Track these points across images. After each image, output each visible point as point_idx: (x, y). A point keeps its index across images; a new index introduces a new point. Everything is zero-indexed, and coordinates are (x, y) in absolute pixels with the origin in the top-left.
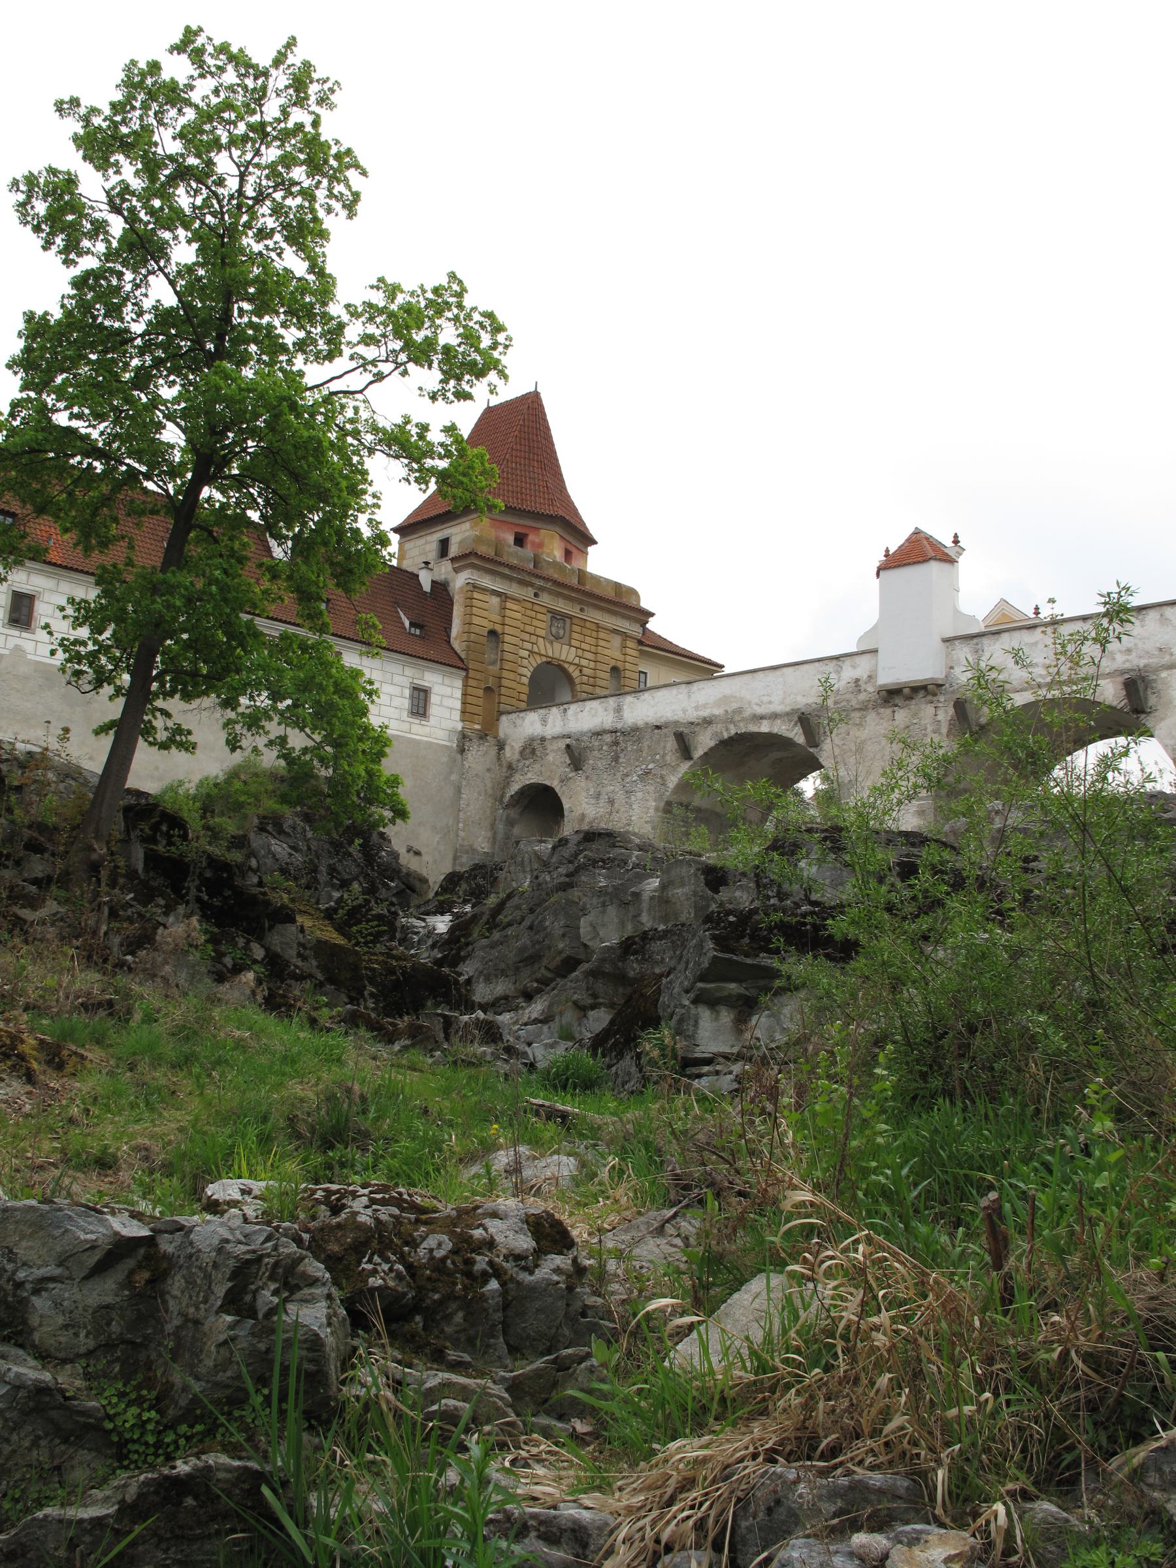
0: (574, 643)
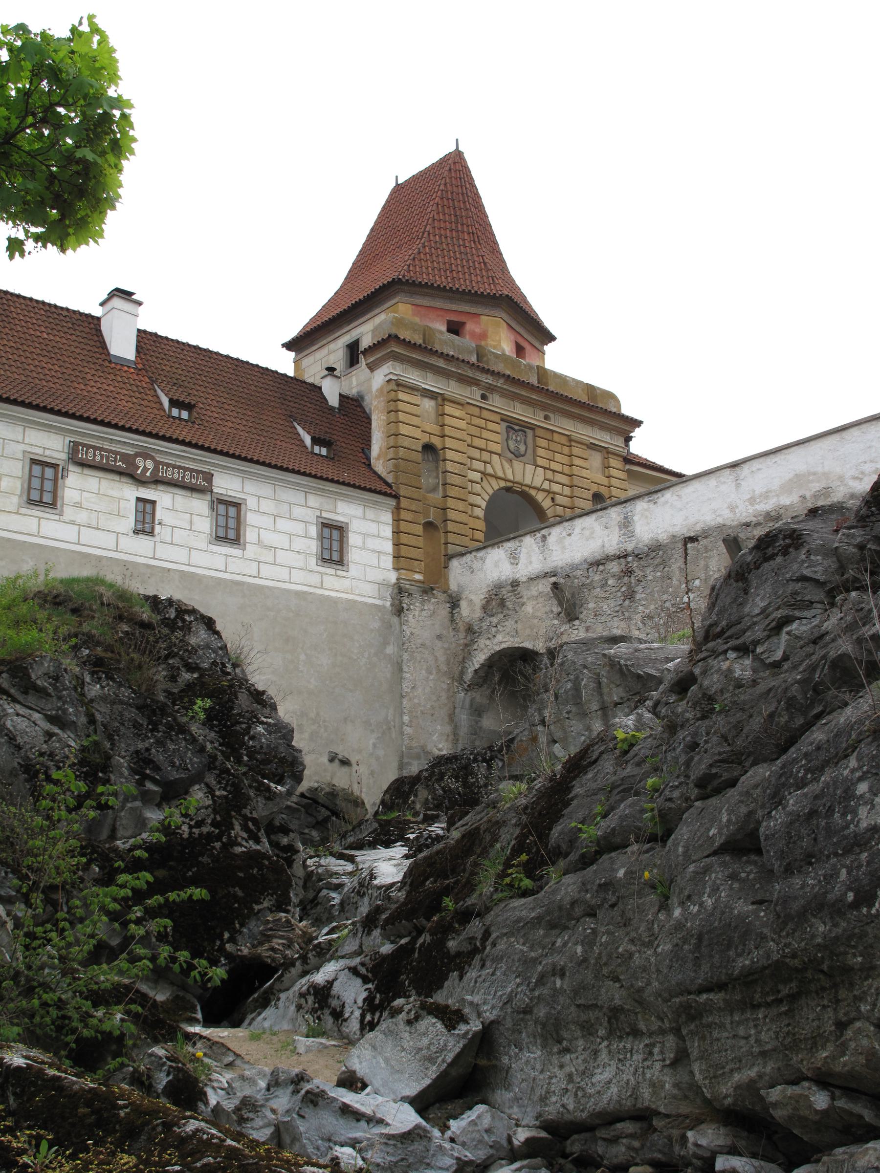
0: (540, 461)
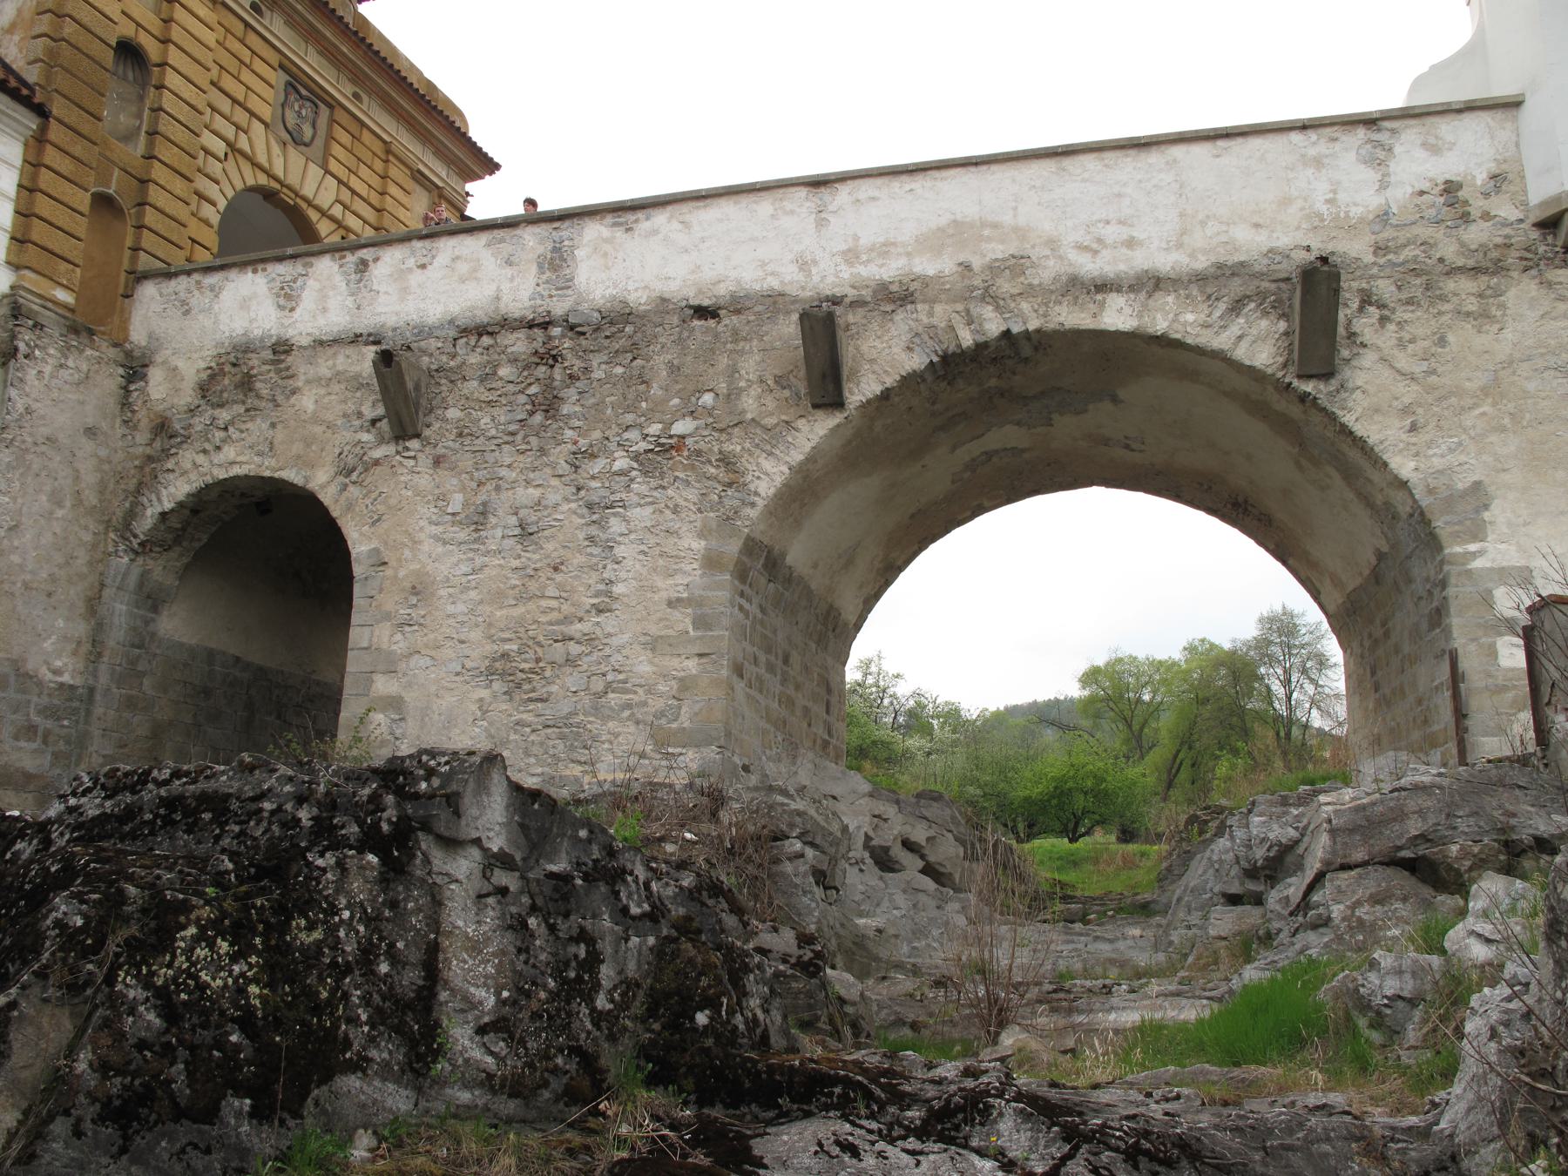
0: (333, 166)
